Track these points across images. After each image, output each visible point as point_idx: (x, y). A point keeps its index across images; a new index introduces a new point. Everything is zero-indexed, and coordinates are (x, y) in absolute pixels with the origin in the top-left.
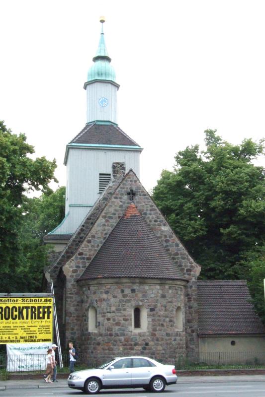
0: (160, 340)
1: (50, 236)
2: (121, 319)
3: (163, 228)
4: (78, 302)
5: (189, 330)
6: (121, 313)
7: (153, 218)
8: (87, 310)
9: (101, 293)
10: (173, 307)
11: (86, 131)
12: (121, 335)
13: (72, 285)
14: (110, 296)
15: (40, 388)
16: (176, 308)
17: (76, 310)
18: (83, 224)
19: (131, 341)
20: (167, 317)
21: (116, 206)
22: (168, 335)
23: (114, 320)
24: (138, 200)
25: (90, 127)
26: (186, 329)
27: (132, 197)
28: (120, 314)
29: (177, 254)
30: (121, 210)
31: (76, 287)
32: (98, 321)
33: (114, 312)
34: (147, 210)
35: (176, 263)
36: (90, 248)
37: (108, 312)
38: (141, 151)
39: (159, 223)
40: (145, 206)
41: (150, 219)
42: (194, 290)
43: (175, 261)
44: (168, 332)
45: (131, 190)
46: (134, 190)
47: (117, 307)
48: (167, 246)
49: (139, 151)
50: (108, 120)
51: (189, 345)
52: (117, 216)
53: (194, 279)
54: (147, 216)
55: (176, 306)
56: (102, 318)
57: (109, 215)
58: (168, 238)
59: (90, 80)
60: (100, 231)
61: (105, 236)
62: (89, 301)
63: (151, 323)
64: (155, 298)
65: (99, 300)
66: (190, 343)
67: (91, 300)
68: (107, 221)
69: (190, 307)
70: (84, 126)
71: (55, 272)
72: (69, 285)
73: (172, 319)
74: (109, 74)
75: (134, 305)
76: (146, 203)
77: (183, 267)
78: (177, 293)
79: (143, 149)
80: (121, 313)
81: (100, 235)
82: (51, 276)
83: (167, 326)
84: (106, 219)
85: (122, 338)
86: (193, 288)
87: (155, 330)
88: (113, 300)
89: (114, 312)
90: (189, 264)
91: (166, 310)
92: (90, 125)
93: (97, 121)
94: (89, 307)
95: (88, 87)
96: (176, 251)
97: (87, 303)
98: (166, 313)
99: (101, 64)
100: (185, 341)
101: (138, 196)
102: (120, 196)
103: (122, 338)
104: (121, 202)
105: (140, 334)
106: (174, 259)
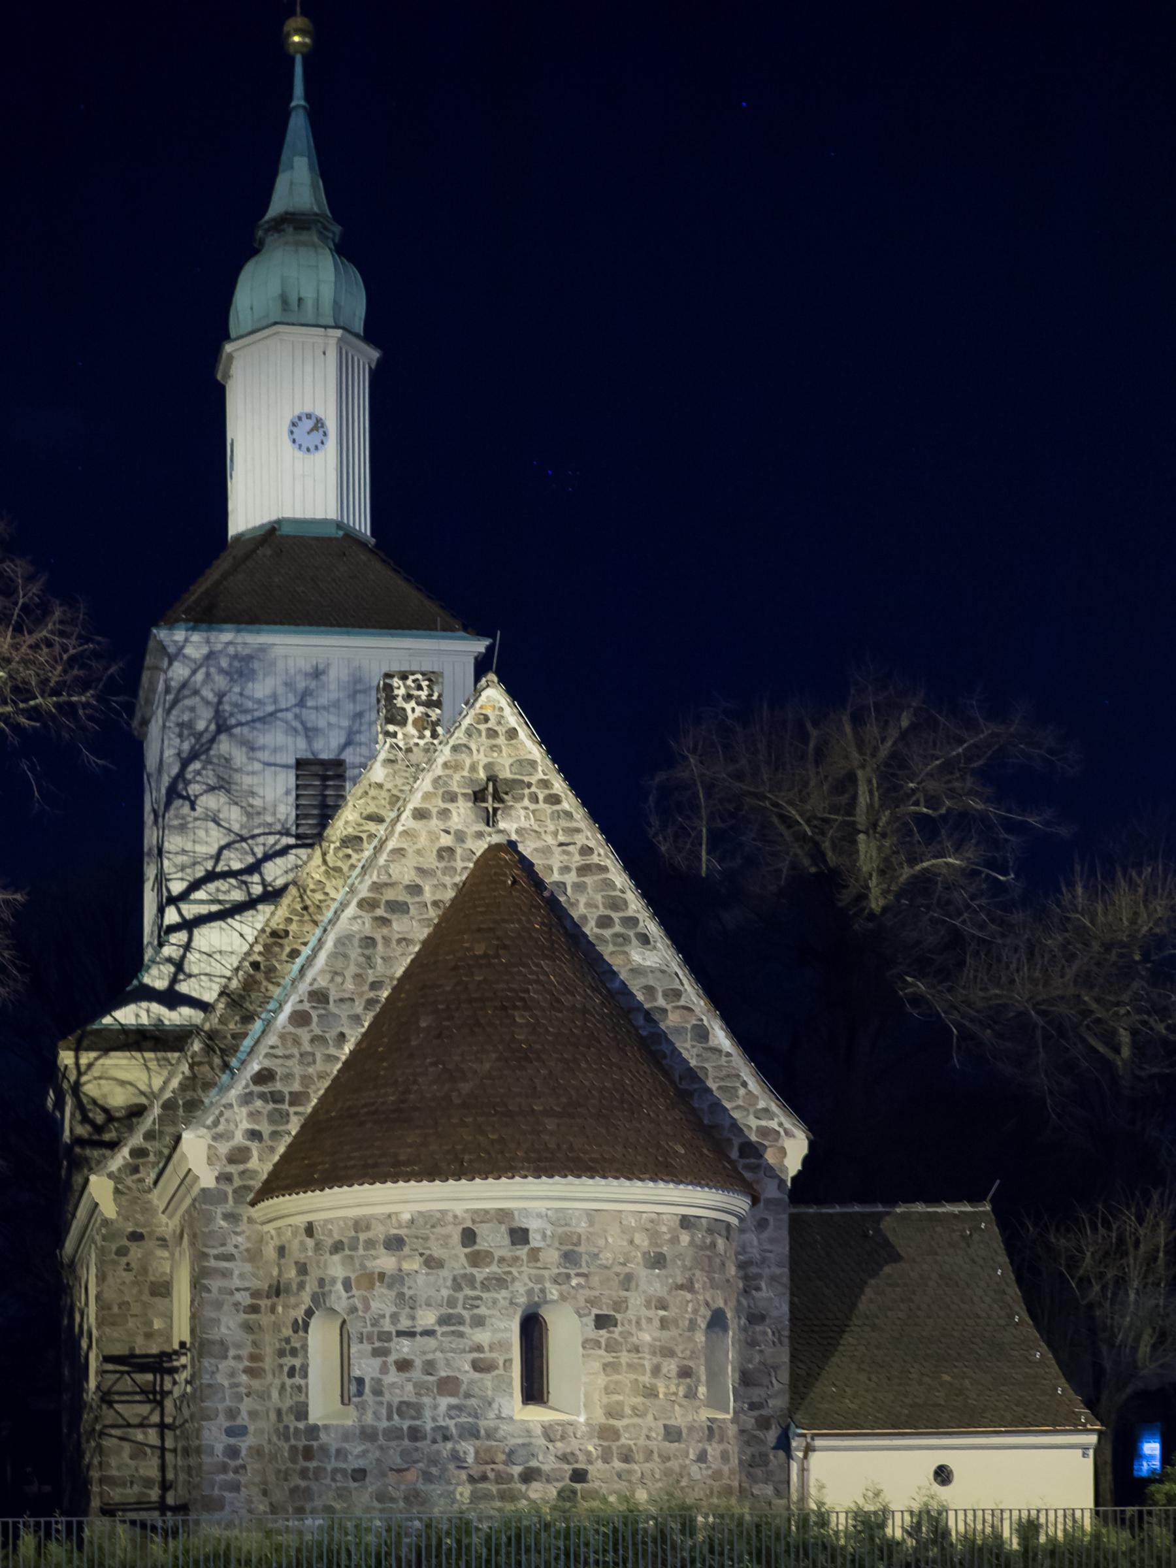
0: (639, 1457)
4: (256, 1294)
6: (461, 1335)
20: (669, 1353)
37: (400, 1334)
38: (97, 1205)
56: (377, 1362)
57: (389, 895)
61: (372, 995)
67: (321, 1282)
82: (117, 1191)
84: (380, 912)
87: (613, 1412)
94: (309, 1313)
101: (526, 802)
103: (468, 1449)
105: (549, 1433)
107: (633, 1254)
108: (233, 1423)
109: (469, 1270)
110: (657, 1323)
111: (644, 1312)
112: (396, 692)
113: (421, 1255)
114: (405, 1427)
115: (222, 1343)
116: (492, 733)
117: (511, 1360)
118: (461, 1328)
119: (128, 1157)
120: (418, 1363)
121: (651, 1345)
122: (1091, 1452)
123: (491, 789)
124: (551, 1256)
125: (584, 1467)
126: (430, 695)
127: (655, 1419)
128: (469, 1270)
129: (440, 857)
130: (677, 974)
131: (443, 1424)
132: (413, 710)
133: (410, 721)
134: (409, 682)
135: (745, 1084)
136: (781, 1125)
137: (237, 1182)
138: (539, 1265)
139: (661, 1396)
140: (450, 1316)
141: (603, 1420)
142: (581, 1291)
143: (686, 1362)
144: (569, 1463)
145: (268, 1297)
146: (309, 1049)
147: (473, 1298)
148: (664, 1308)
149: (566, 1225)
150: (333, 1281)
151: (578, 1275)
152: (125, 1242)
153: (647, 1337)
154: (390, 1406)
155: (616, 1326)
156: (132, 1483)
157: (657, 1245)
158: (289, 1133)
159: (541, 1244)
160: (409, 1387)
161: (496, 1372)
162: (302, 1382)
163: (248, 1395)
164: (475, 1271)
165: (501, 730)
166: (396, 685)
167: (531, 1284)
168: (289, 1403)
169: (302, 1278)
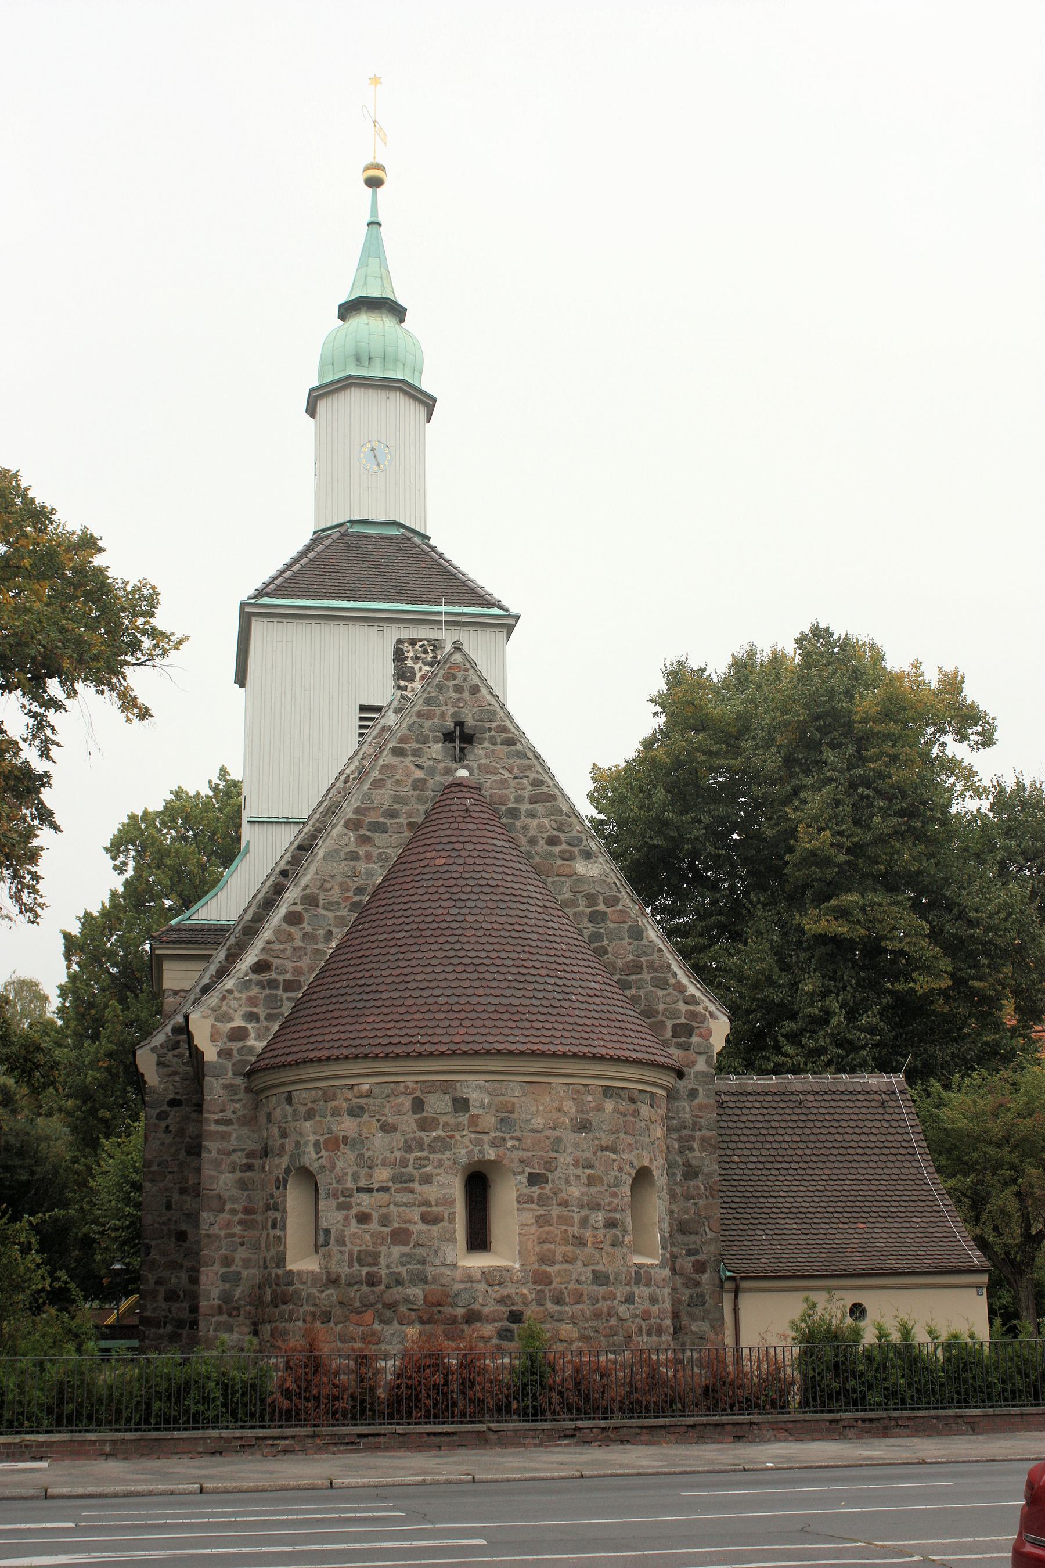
1: (176, 929)
2: (415, 1213)
3: (581, 867)
4: (250, 1155)
5: (687, 1264)
6: (412, 1192)
7: (541, 828)
8: (281, 1184)
9: (336, 1113)
10: (620, 1169)
11: (312, 555)
12: (413, 1283)
13: (226, 1087)
14: (369, 1125)
15: (54, 1497)
16: (634, 1172)
17: (243, 1185)
18: (282, 865)
19: (454, 1305)
20: (596, 1207)
21: (398, 782)
22: (600, 1278)
23: (385, 1221)
24: (483, 761)
25: (327, 542)
26: (674, 1257)
27: (462, 750)
28: (407, 1198)
29: (637, 968)
30: (419, 799)
31: (241, 1095)
32: (323, 1224)
33: (384, 1189)
34: (519, 800)
35: (635, 1000)
36: (298, 943)
37: (359, 1190)
38: (510, 629)
39: (564, 846)
40: (512, 783)
41: (532, 832)
42: (702, 1107)
43: (627, 993)
44: (599, 1268)
45: (456, 724)
46: (470, 722)
47: (398, 1170)
48: (596, 937)
49: (507, 624)
50: (392, 519)
51: (685, 1321)
52: (403, 820)
53: (701, 1065)
54: (518, 824)
55: (631, 1164)
56: (340, 1215)
58: (602, 907)
59: (330, 379)
60: (339, 879)
61: (356, 899)
62: (289, 1146)
63: (533, 1229)
64: (549, 1133)
65: (326, 1142)
66: (690, 1315)
68: (364, 840)
69: (691, 1172)
70: (306, 539)
71: (174, 1049)
72: (215, 1089)
73: (617, 1216)
74: (396, 360)
75: (464, 1160)
76: (516, 772)
77: (660, 1017)
78: (636, 1113)
79: (517, 618)
80: (412, 1192)
81: (336, 893)
82: (159, 1064)
83: (598, 1245)
84: (362, 832)
85: (416, 1292)
86: (701, 1099)
87: (546, 1259)
88: (379, 1142)
89: (384, 1189)
90: (682, 1007)
91: (591, 1181)
92: (329, 536)
93: (351, 522)
94: (288, 1171)
95: (322, 406)
96: (631, 957)
97: (280, 1155)
98: (593, 1190)
99: (364, 323)
100: (668, 1306)
101: (486, 744)
102: (415, 746)
104: (419, 767)
105: (490, 1278)
106: (624, 985)
107: (561, 1120)
108: (228, 1270)
109: (418, 1134)
110: (584, 1179)
111: (572, 1171)
112: (406, 654)
113: (378, 1120)
114: (364, 1273)
115: (219, 1197)
116: (458, 689)
117: (454, 1213)
118: (411, 1185)
119: (170, 1034)
120: (375, 1216)
121: (578, 1199)
122: (985, 1291)
123: (458, 733)
124: (489, 1121)
125: (520, 1309)
126: (435, 657)
127: (585, 1265)
128: (418, 1134)
129: (415, 787)
130: (615, 883)
131: (396, 1270)
132: (420, 669)
133: (418, 678)
134: (417, 647)
135: (675, 975)
136: (706, 1009)
137: (237, 1057)
138: (478, 1129)
139: (589, 1245)
140: (402, 1174)
141: (536, 1266)
142: (515, 1152)
143: (612, 1215)
144: (506, 1305)
145: (261, 1158)
146: (301, 944)
147: (420, 1158)
148: (591, 1167)
149: (502, 1095)
150: (307, 1143)
151: (512, 1138)
152: (165, 1108)
153: (575, 1191)
154: (351, 1255)
155: (547, 1182)
156: (165, 1323)
157: (582, 1112)
158: (282, 1015)
159: (480, 1112)
160: (367, 1237)
161: (442, 1224)
162: (282, 1234)
163: (242, 1244)
164: (423, 1134)
165: (466, 686)
166: (406, 649)
167: (471, 1147)
168: (273, 1252)
169: (283, 1140)
